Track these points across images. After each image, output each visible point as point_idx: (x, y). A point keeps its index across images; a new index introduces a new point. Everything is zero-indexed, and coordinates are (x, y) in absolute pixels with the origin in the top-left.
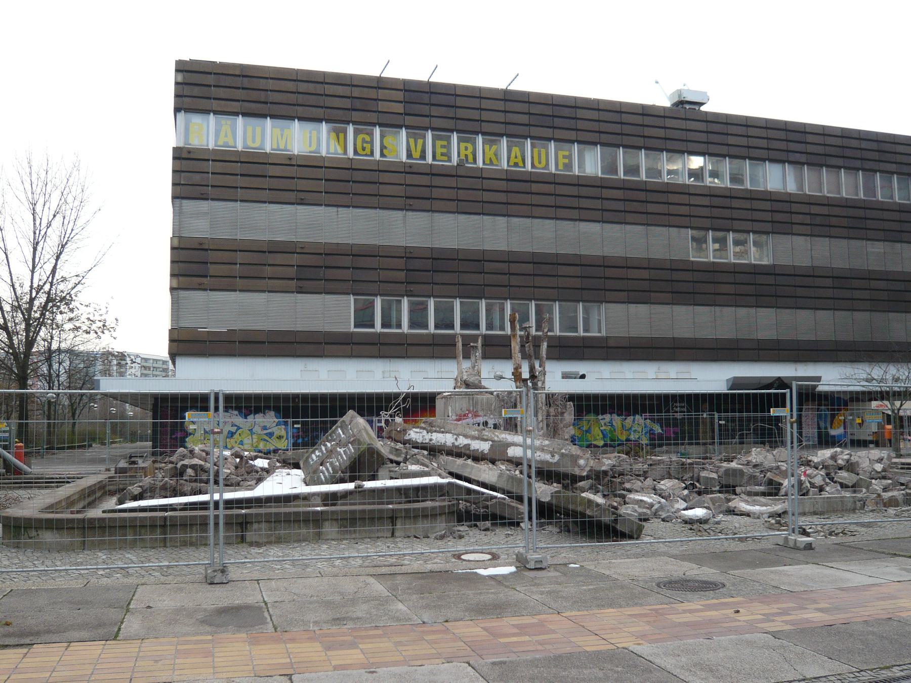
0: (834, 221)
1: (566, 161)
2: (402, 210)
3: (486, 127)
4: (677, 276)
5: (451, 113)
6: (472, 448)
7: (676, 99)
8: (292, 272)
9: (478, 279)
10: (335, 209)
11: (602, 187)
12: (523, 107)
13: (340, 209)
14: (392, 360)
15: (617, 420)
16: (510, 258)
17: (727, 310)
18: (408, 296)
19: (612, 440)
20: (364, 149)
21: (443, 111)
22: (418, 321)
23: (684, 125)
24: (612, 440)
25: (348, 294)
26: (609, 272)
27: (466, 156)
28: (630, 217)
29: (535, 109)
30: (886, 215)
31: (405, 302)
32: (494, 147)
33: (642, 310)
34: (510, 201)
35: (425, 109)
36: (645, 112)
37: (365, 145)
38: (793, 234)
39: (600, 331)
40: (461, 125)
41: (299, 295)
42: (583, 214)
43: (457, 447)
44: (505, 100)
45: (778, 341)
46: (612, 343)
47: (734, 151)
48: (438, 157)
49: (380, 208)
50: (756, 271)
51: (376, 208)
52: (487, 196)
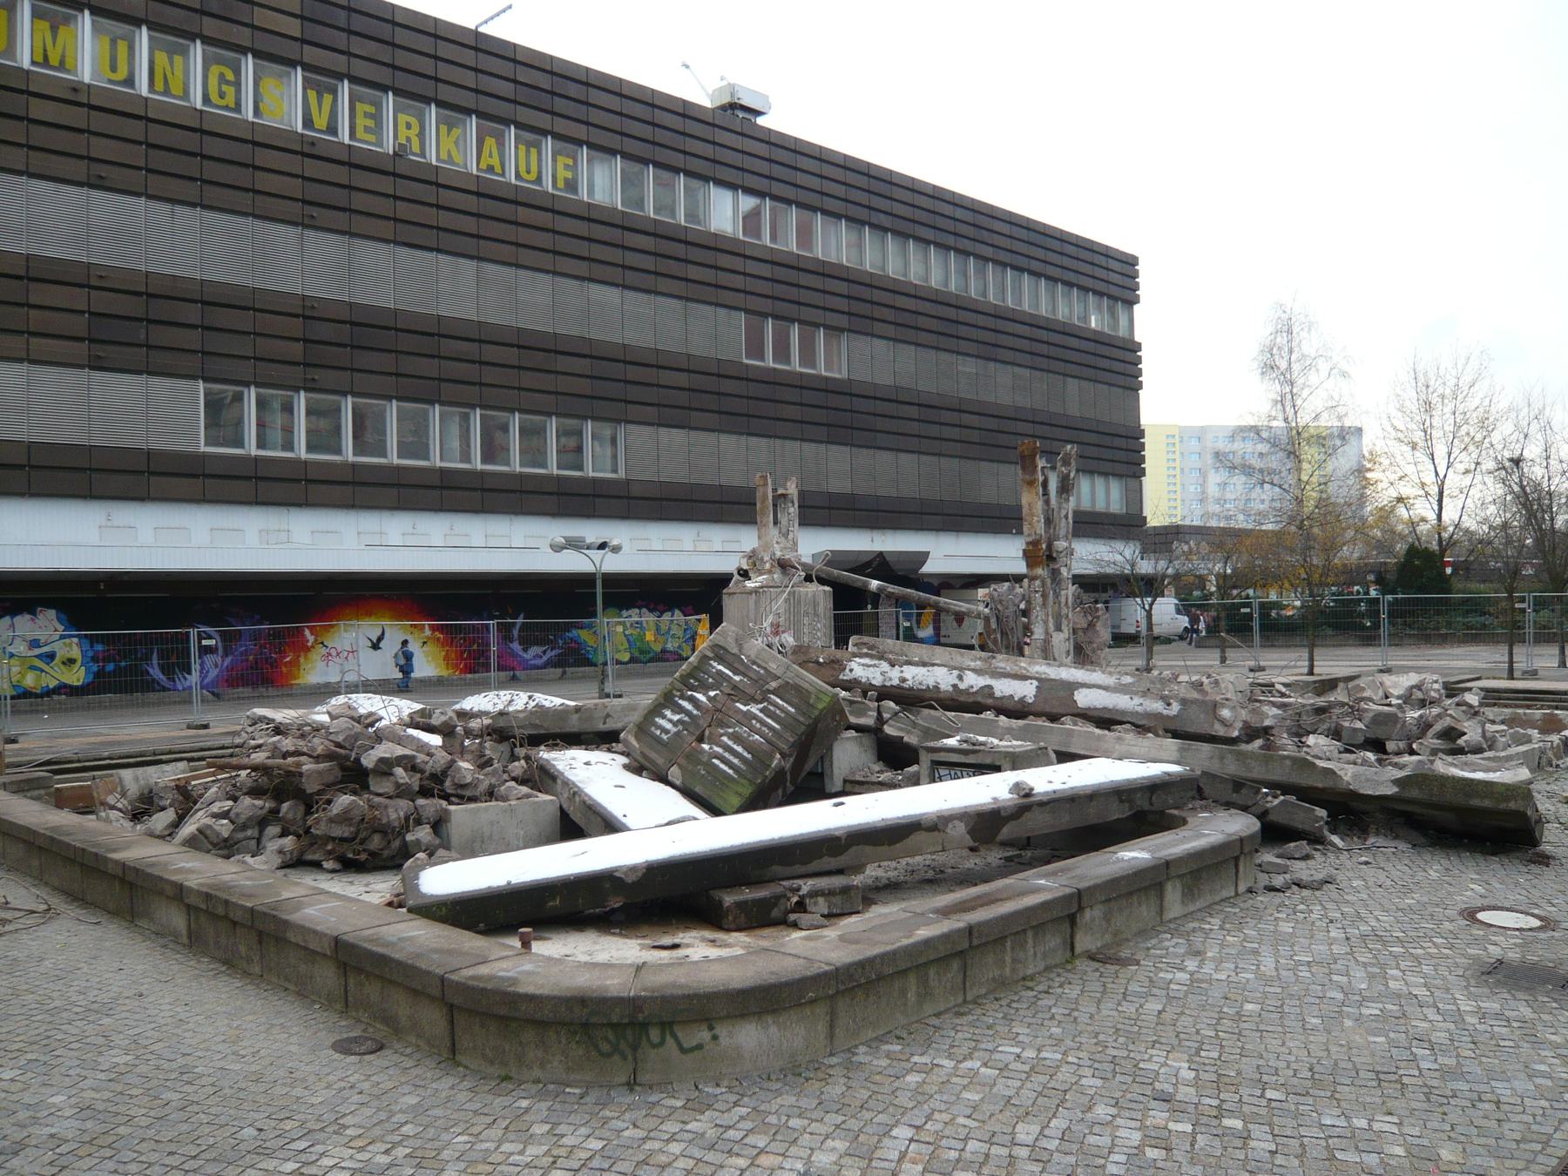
0: (923, 322)
1: (569, 175)
2: (295, 224)
3: (445, 93)
4: (728, 386)
5: (385, 54)
6: (998, 694)
7: (726, 100)
8: (79, 325)
9: (429, 367)
10: (166, 207)
11: (624, 228)
12: (505, 68)
13: (178, 209)
14: (292, 510)
15: (649, 618)
16: (481, 336)
17: (790, 445)
18: (306, 390)
19: (642, 652)
20: (222, 95)
21: (370, 49)
22: (323, 439)
23: (723, 141)
24: (642, 652)
25: (195, 378)
26: (633, 373)
27: (409, 139)
28: (664, 284)
29: (524, 75)
30: (752, 267)
31: (251, 395)
32: (456, 132)
33: (674, 438)
34: (482, 233)
35: (340, 39)
36: (685, 110)
37: (224, 88)
38: (873, 335)
39: (615, 471)
40: (402, 80)
41: (96, 375)
42: (595, 271)
43: (966, 692)
44: (476, 49)
45: (852, 497)
46: (636, 491)
47: (803, 196)
48: (360, 133)
49: (255, 216)
50: (827, 388)
51: (245, 214)
52: (445, 219)
